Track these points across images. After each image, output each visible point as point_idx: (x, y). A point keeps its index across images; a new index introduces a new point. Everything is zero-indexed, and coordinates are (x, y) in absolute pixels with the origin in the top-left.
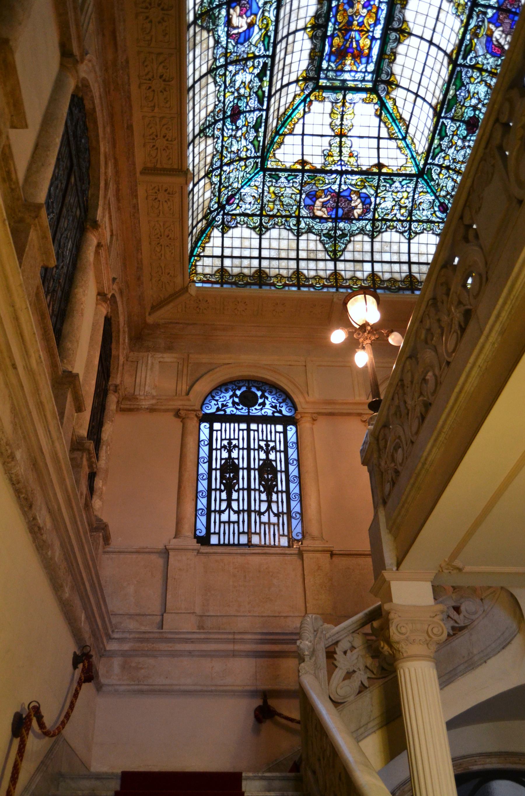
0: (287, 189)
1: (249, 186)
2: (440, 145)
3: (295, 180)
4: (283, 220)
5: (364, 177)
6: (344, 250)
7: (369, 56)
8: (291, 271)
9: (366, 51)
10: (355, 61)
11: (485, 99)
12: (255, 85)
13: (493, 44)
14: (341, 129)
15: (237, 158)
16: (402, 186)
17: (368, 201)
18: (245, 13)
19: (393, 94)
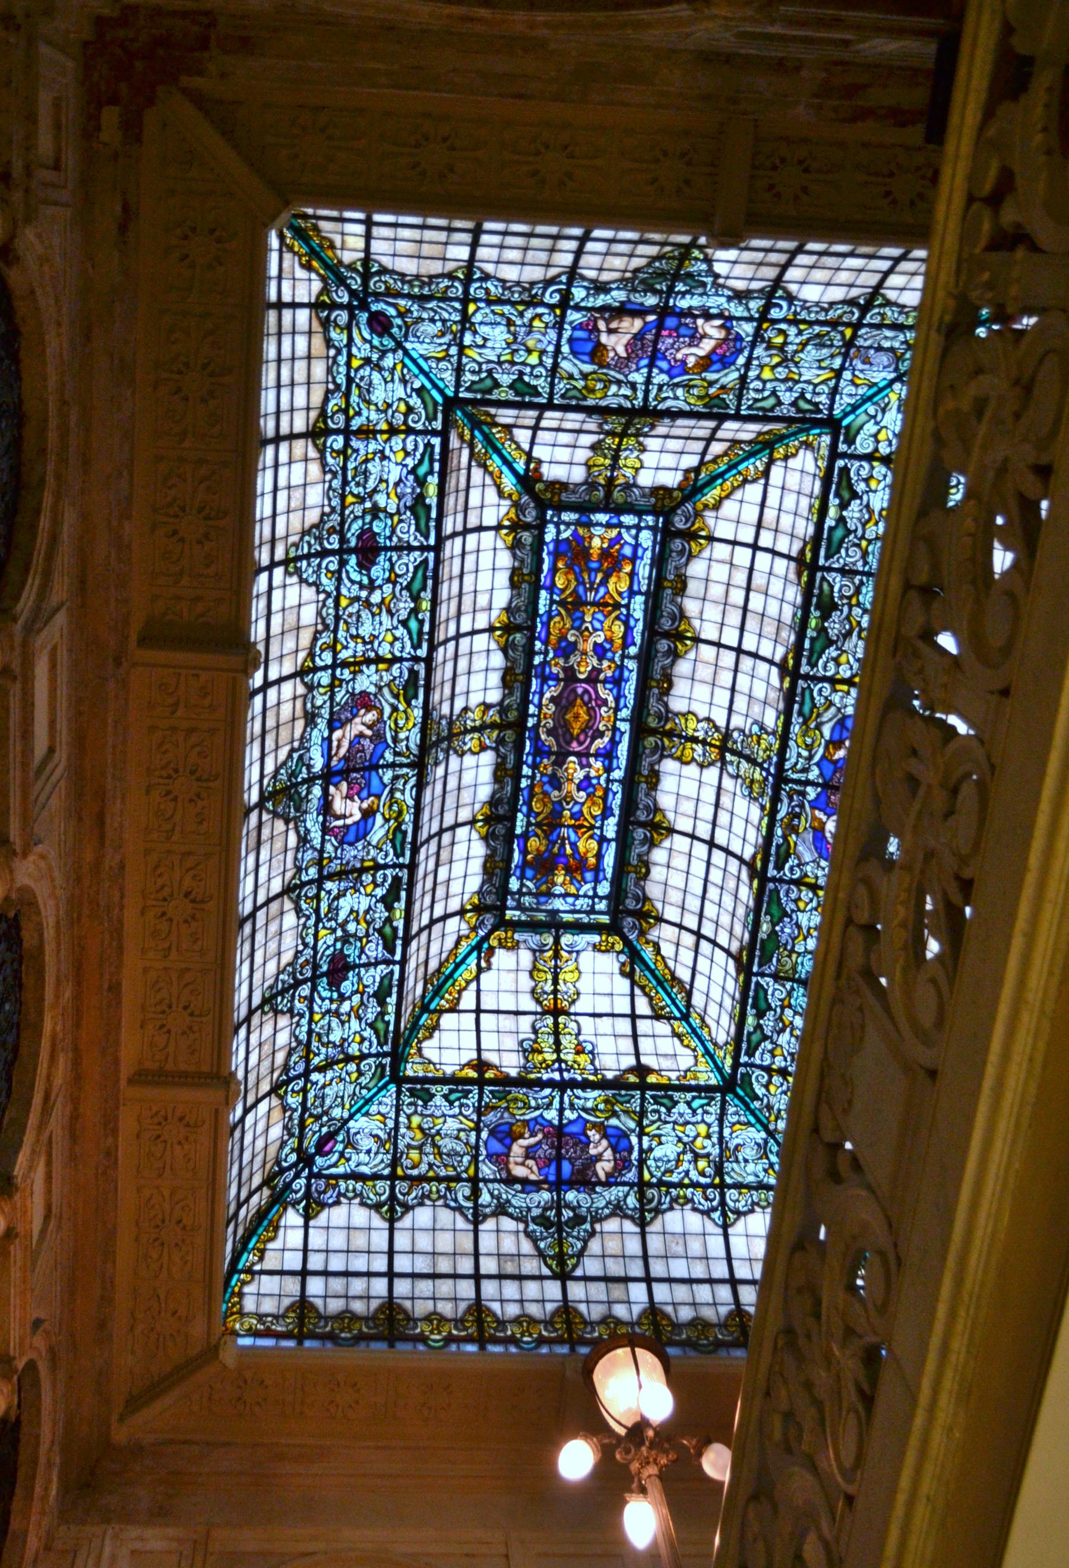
0: (449, 1120)
1: (367, 1114)
4: (442, 1187)
5: (610, 1093)
6: (580, 1254)
7: (598, 869)
8: (463, 1306)
10: (572, 878)
14: (555, 999)
17: (623, 1143)
19: (653, 934)
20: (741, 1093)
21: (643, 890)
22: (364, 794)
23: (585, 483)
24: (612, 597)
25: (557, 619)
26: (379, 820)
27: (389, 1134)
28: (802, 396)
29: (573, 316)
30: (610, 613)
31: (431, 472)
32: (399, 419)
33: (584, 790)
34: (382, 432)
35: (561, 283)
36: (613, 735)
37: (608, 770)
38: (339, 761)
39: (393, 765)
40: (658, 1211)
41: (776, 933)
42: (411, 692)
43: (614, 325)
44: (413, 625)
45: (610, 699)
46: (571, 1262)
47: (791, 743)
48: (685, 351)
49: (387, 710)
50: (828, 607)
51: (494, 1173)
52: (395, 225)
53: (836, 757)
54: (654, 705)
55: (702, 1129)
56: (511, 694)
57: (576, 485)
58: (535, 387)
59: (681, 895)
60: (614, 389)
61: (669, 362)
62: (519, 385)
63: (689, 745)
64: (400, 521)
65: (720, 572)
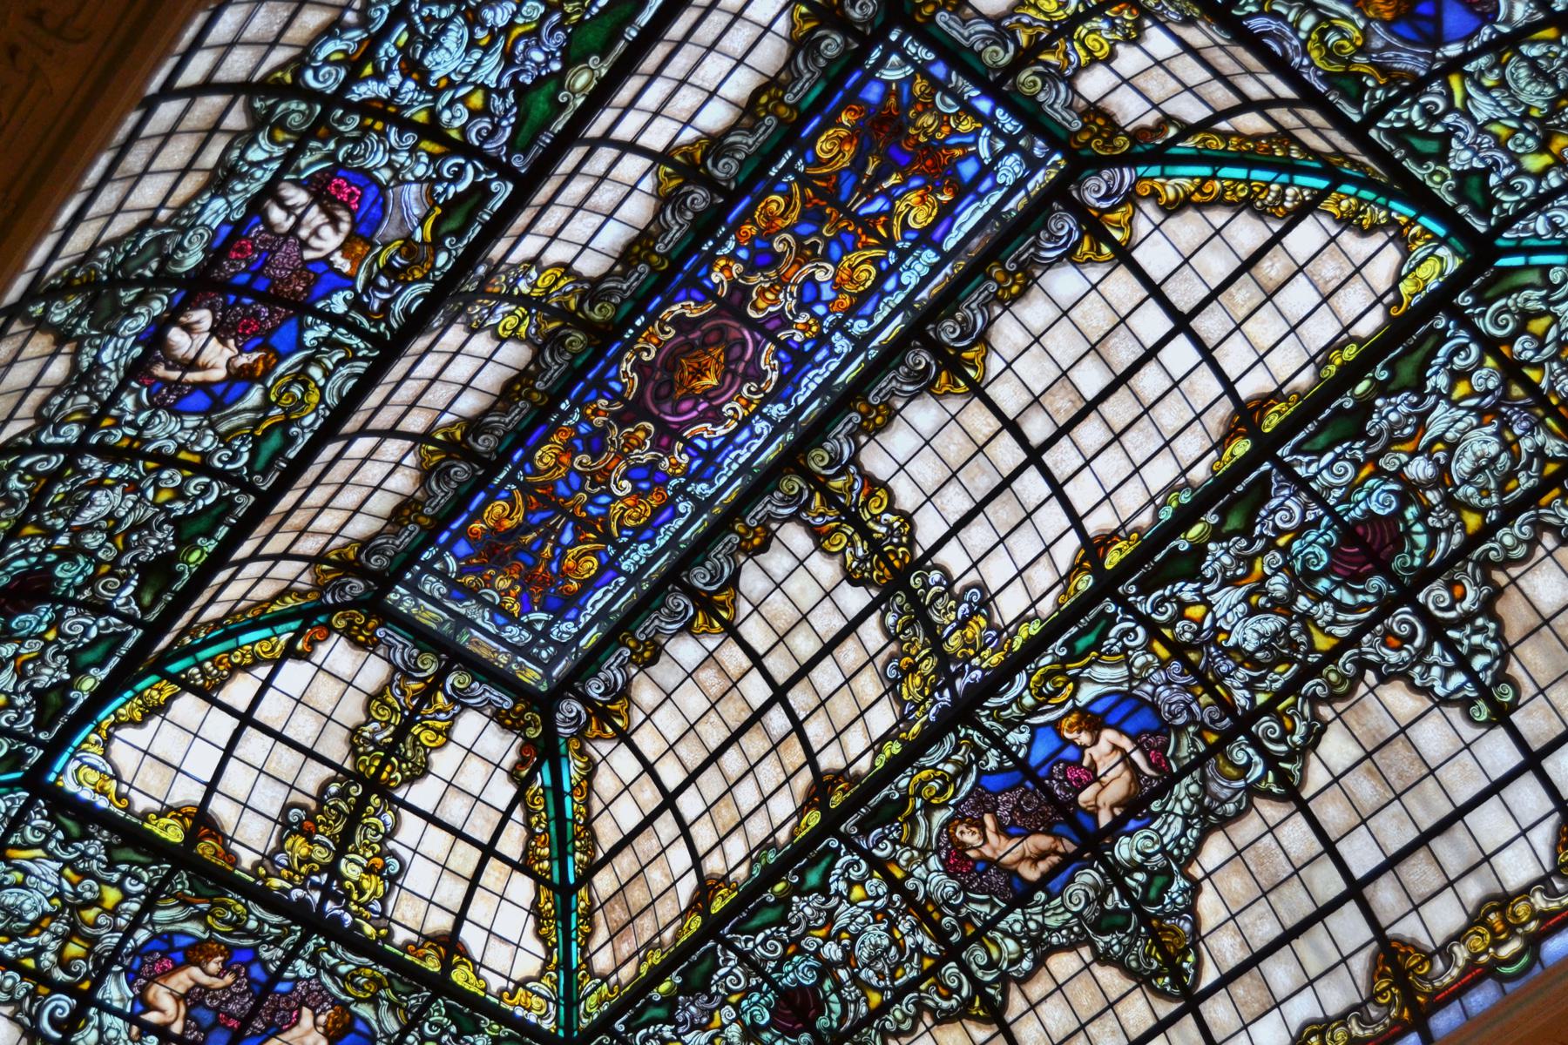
0: (1481, 117)
3: (1419, 122)
10: (903, 108)
11: (449, 20)
12: (1226, 560)
22: (1069, 753)
24: (526, 502)
25: (631, 523)
26: (1086, 693)
30: (543, 485)
39: (998, 742)
41: (563, 60)
42: (889, 810)
44: (813, 878)
45: (626, 366)
47: (332, 400)
48: (219, 983)
49: (939, 817)
50: (158, 572)
53: (256, 355)
57: (479, 710)
60: (343, 969)
61: (247, 975)
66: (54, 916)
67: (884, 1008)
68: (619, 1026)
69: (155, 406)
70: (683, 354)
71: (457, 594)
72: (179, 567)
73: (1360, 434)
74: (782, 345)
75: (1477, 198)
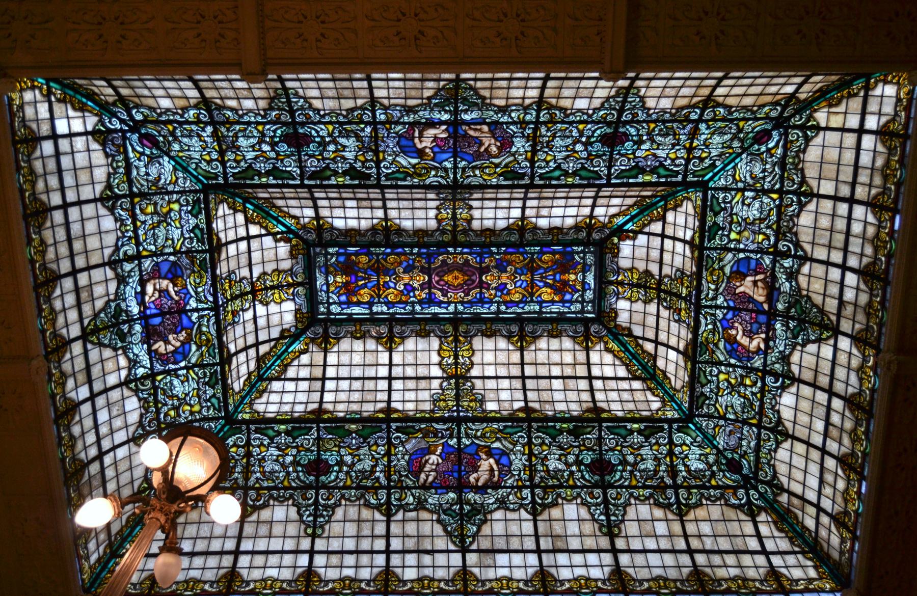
1: (175, 169)
2: (279, 433)
4: (130, 234)
5: (215, 341)
6: (101, 345)
7: (349, 303)
8: (54, 266)
9: (355, 299)
10: (341, 288)
13: (422, 458)
15: (224, 147)
16: (209, 400)
17: (179, 357)
18: (437, 145)
19: (313, 348)
20: (226, 429)
21: (345, 337)
22: (437, 150)
23: (619, 268)
24: (537, 291)
25: (521, 258)
27: (163, 188)
28: (708, 398)
29: (767, 260)
30: (527, 291)
31: (659, 177)
32: (697, 153)
33: (405, 288)
34: (691, 143)
35: (796, 251)
36: (444, 303)
37: (420, 302)
38: (465, 131)
40: (136, 391)
42: (509, 176)
43: (760, 284)
44: (557, 173)
45: (470, 298)
46: (94, 339)
47: (485, 425)
48: (740, 328)
49: (496, 161)
50: (575, 433)
51: (146, 270)
52: (492, 80)
54: (473, 328)
55: (197, 408)
56: (477, 235)
57: (617, 263)
58: (714, 238)
59: (348, 362)
62: (716, 228)
63: (452, 353)
64: (629, 159)
65: (568, 358)
66: (739, 393)
67: (580, 122)
68: (680, 178)
69: (510, 471)
70: (454, 286)
71: (587, 287)
72: (571, 427)
73: (275, 168)
74: (429, 263)
75: (197, 207)
